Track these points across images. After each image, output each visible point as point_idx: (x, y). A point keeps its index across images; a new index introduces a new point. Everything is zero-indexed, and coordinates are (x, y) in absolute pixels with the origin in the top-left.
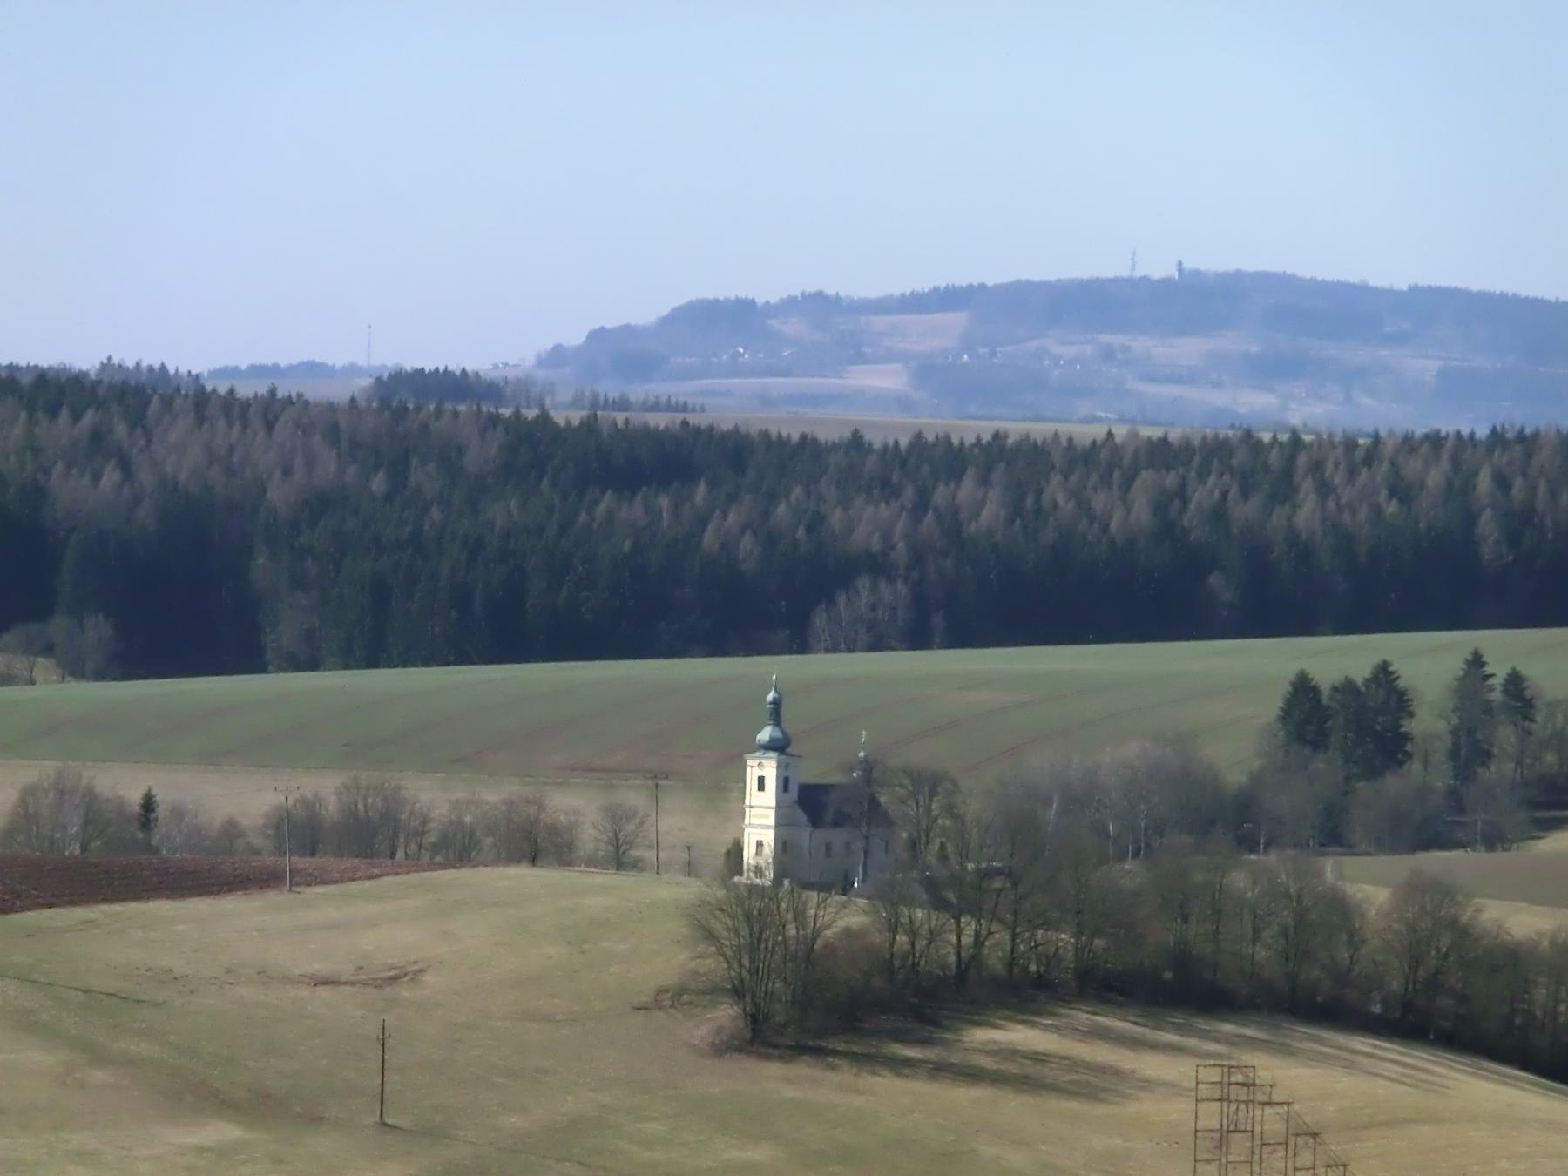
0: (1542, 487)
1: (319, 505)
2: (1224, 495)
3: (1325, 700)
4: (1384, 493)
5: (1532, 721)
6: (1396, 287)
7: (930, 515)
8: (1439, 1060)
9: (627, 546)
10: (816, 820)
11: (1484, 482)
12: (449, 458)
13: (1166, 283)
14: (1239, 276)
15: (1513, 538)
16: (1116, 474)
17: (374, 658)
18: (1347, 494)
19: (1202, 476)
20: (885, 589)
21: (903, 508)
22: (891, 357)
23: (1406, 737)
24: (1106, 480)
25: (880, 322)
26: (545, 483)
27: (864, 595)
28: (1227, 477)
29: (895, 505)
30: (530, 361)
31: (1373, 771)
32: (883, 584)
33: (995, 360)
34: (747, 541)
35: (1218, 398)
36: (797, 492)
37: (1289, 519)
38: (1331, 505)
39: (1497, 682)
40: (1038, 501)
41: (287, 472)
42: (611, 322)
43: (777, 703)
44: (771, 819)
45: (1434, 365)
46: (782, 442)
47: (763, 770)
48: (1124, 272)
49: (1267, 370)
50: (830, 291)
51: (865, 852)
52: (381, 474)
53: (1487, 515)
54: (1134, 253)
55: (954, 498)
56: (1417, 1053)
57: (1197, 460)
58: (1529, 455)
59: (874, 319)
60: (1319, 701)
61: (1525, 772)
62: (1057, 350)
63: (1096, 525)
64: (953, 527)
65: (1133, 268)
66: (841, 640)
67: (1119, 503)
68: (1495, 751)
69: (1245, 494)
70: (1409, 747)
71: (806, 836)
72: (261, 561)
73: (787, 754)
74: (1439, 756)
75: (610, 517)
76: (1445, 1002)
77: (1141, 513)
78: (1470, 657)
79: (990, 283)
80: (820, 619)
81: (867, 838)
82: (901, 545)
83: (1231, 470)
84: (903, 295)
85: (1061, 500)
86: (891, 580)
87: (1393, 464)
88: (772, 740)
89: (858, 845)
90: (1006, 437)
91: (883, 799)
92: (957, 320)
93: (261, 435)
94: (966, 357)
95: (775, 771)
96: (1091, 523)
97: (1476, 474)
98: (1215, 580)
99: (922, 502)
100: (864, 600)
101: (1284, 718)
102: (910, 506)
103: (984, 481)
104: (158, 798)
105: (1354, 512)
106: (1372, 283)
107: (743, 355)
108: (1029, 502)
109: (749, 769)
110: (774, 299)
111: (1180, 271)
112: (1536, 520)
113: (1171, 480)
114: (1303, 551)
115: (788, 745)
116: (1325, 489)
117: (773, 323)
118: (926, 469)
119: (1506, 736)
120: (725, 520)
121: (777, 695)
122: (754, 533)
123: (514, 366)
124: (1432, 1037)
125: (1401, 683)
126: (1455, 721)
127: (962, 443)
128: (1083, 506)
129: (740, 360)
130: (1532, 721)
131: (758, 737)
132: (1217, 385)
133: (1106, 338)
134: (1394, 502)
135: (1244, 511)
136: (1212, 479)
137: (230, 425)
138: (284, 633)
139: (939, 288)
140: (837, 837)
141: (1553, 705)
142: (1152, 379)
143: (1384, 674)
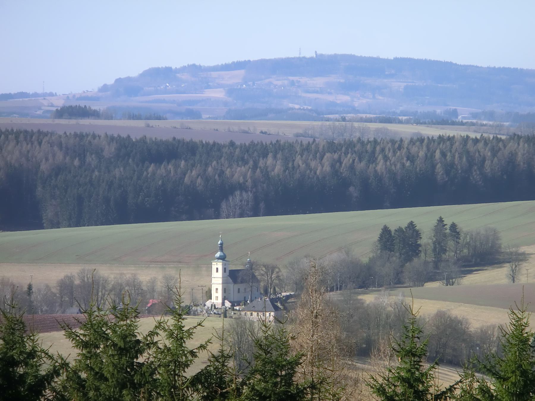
0: (457, 156)
1: (58, 170)
2: (354, 161)
3: (393, 234)
4: (405, 159)
5: (460, 239)
6: (389, 58)
7: (258, 170)
8: (449, 370)
9: (160, 183)
10: (235, 281)
11: (438, 154)
12: (98, 152)
13: (311, 58)
14: (336, 56)
15: (447, 172)
16: (318, 154)
17: (78, 223)
18: (393, 160)
19: (346, 153)
20: (244, 195)
21: (250, 168)
22: (219, 86)
23: (420, 245)
24: (315, 157)
25: (214, 74)
26: (130, 160)
27: (237, 198)
28: (354, 155)
29: (247, 167)
30: (96, 90)
31: (409, 259)
32: (244, 193)
33: (254, 86)
34: (199, 180)
35: (330, 98)
36: (214, 163)
37: (375, 168)
38: (388, 163)
39: (448, 227)
40: (293, 164)
41: (47, 159)
42: (123, 76)
43: (221, 244)
44: (220, 281)
45: (403, 85)
46: (207, 144)
47: (217, 267)
48: (297, 55)
49: (346, 88)
50: (197, 64)
51: (251, 292)
52: (77, 159)
53: (439, 165)
54: (300, 49)
55: (266, 164)
56: (444, 369)
57: (344, 149)
58: (452, 145)
59: (212, 73)
60: (391, 235)
61: (458, 255)
62: (276, 82)
63: (312, 172)
64: (266, 174)
65: (300, 54)
66: (231, 212)
67: (319, 164)
68: (448, 249)
69: (360, 160)
70: (420, 249)
71: (231, 286)
72: (39, 189)
73: (225, 261)
74: (430, 251)
75: (154, 174)
76: (449, 351)
77: (327, 168)
78: (439, 219)
79: (251, 60)
80: (224, 205)
81: (252, 287)
82: (249, 180)
83: (355, 152)
84: (222, 65)
85: (301, 164)
86: (247, 192)
87: (407, 149)
88: (220, 256)
89: (249, 289)
90: (280, 141)
91: (256, 274)
92: (241, 73)
93: (38, 147)
94: (244, 85)
95: (221, 266)
96: (311, 171)
97: (435, 152)
98: (351, 189)
99: (255, 166)
100: (238, 198)
101: (380, 240)
102: (252, 167)
103: (275, 157)
104: (33, 286)
105: (395, 165)
106: (381, 57)
107: (168, 86)
108: (290, 165)
109: (213, 266)
110: (178, 67)
111: (316, 54)
112: (455, 167)
113: (336, 156)
114: (379, 178)
115: (225, 258)
116: (386, 158)
117: (178, 75)
118: (256, 154)
119: (451, 244)
120: (192, 173)
121: (221, 242)
122: (201, 177)
123: (90, 92)
124: (445, 362)
125: (417, 228)
126: (435, 239)
127: (266, 144)
128: (308, 165)
129: (168, 88)
130: (460, 239)
131: (216, 255)
132: (330, 93)
133: (291, 78)
134: (409, 162)
135: (360, 166)
136: (349, 155)
137: (28, 144)
138: (49, 213)
139: (235, 62)
140: (242, 287)
141: (466, 234)
142: (308, 92)
143: (411, 225)
